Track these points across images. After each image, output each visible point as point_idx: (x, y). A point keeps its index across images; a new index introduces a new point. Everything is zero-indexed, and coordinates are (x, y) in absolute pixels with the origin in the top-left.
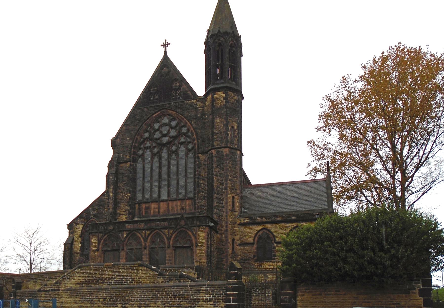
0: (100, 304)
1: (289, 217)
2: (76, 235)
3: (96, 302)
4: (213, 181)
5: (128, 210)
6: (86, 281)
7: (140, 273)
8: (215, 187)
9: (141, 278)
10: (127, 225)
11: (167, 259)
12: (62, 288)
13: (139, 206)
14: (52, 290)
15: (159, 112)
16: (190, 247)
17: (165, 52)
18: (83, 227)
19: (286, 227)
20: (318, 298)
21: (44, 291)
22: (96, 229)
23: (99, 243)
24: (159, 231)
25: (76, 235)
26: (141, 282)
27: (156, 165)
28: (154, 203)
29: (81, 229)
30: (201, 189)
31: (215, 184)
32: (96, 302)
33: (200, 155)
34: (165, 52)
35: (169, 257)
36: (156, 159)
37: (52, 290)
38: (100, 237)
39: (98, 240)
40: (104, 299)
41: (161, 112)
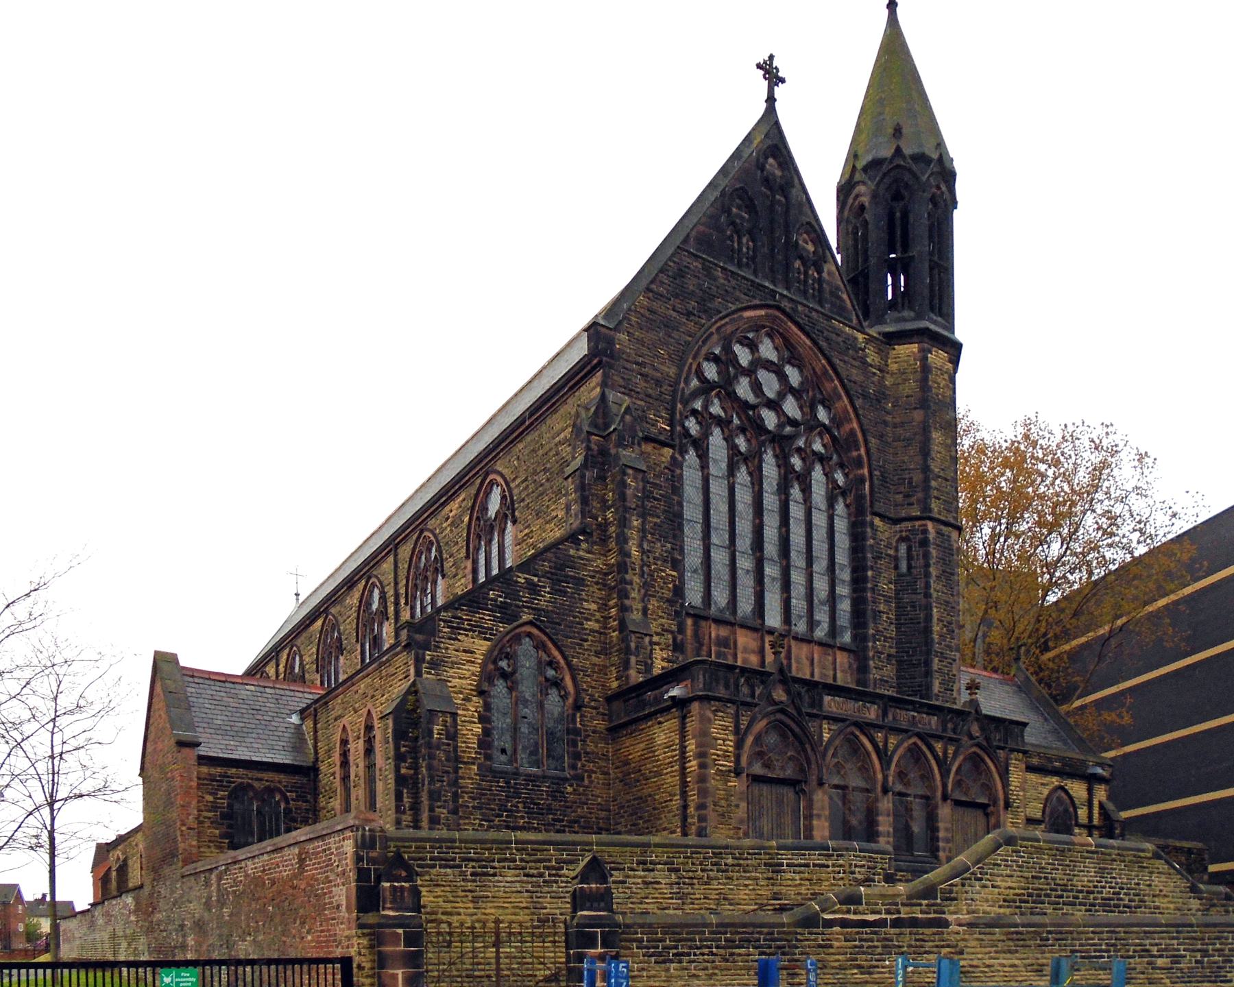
0: (1158, 975)
1: (1050, 760)
2: (456, 682)
3: (1139, 968)
4: (929, 617)
5: (672, 632)
6: (1030, 895)
7: (1156, 880)
8: (935, 637)
9: (1158, 896)
10: (827, 699)
11: (941, 834)
12: (956, 915)
13: (695, 624)
14: (897, 923)
15: (763, 312)
16: (983, 807)
17: (771, 100)
18: (490, 651)
19: (1042, 784)
20: (703, 954)
21: (844, 923)
22: (727, 687)
23: (739, 745)
24: (919, 743)
25: (456, 682)
26: (1158, 908)
27: (744, 497)
28: (749, 633)
29: (480, 659)
30: (881, 628)
31: (936, 628)
32: (1139, 968)
33: (877, 521)
34: (771, 100)
35: (947, 830)
36: (742, 476)
37: (897, 923)
38: (744, 722)
39: (737, 731)
40: (1176, 959)
41: (767, 315)
